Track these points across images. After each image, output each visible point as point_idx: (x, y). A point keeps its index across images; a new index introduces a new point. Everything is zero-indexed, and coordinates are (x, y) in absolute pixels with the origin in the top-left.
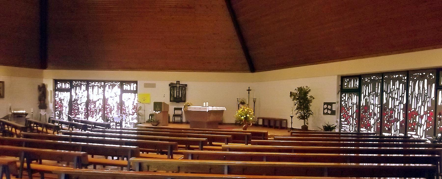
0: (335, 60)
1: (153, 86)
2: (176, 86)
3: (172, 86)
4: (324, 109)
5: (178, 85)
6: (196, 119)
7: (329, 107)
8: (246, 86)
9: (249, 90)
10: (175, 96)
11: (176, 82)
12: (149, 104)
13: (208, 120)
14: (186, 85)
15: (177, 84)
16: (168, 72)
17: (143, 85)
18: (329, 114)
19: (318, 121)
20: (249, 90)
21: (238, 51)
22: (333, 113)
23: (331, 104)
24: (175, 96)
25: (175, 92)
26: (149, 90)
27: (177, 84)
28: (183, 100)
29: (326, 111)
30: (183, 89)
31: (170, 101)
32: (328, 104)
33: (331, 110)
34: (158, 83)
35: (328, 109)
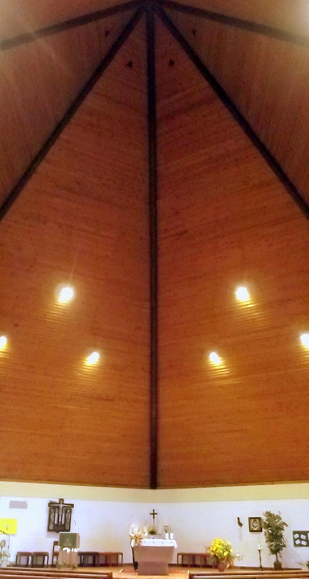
0: (264, 483)
1: (23, 505)
2: (58, 508)
3: (53, 507)
4: (295, 540)
5: (61, 506)
8: (146, 508)
9: (154, 514)
10: (56, 523)
11: (57, 501)
12: (13, 535)
14: (72, 506)
16: (15, 483)
18: (302, 546)
20: (154, 514)
21: (144, 462)
25: (56, 515)
26: (16, 512)
28: (67, 528)
29: (298, 542)
30: (69, 511)
35: (301, 540)
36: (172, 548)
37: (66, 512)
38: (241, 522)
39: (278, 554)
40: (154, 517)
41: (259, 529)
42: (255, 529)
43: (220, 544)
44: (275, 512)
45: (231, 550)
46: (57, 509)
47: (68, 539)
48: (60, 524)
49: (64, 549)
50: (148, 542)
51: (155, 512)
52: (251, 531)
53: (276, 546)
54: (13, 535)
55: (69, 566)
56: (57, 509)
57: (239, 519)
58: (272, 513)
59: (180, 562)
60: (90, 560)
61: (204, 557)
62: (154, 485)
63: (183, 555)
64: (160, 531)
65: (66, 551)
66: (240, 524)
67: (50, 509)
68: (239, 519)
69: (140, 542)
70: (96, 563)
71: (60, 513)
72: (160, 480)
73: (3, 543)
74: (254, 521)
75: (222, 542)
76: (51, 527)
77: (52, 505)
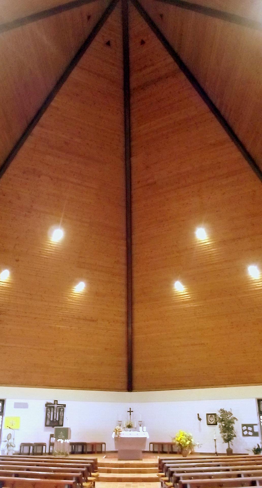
1: (25, 406)
2: (53, 407)
3: (49, 407)
6: (127, 448)
7: (250, 429)
10: (52, 419)
11: (53, 402)
12: (18, 430)
13: (143, 450)
14: (65, 406)
15: (54, 404)
17: (13, 406)
18: (250, 436)
19: (246, 444)
20: (130, 412)
21: (124, 379)
22: (255, 434)
23: (252, 426)
24: (52, 419)
25: (52, 413)
27: (54, 404)
28: (61, 424)
29: (246, 433)
30: (62, 410)
31: (46, 425)
32: (247, 426)
33: (252, 431)
34: (31, 403)
35: (248, 431)
36: (145, 439)
37: (60, 411)
38: (200, 417)
39: (230, 442)
40: (130, 414)
41: (215, 423)
42: (212, 423)
43: (183, 435)
44: (227, 409)
45: (192, 440)
46: (52, 409)
47: (62, 433)
48: (55, 421)
49: (59, 440)
50: (126, 434)
51: (131, 410)
52: (209, 424)
53: (228, 436)
54: (18, 430)
55: (63, 454)
56: (52, 409)
57: (198, 415)
58: (225, 410)
59: (152, 450)
60: (80, 449)
61: (171, 445)
62: (130, 388)
63: (154, 444)
64: (135, 425)
65: (60, 441)
66: (200, 419)
67: (47, 408)
68: (198, 415)
69: (119, 434)
70: (85, 450)
71: (55, 412)
72: (135, 385)
73: (10, 436)
74: (211, 417)
75: (185, 434)
76: (48, 423)
77: (48, 405)
